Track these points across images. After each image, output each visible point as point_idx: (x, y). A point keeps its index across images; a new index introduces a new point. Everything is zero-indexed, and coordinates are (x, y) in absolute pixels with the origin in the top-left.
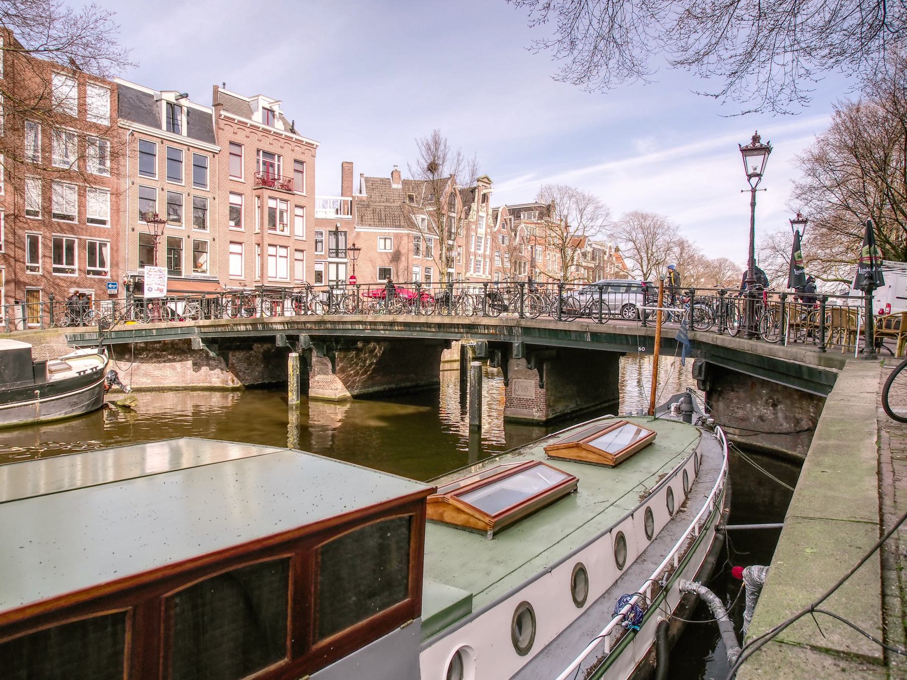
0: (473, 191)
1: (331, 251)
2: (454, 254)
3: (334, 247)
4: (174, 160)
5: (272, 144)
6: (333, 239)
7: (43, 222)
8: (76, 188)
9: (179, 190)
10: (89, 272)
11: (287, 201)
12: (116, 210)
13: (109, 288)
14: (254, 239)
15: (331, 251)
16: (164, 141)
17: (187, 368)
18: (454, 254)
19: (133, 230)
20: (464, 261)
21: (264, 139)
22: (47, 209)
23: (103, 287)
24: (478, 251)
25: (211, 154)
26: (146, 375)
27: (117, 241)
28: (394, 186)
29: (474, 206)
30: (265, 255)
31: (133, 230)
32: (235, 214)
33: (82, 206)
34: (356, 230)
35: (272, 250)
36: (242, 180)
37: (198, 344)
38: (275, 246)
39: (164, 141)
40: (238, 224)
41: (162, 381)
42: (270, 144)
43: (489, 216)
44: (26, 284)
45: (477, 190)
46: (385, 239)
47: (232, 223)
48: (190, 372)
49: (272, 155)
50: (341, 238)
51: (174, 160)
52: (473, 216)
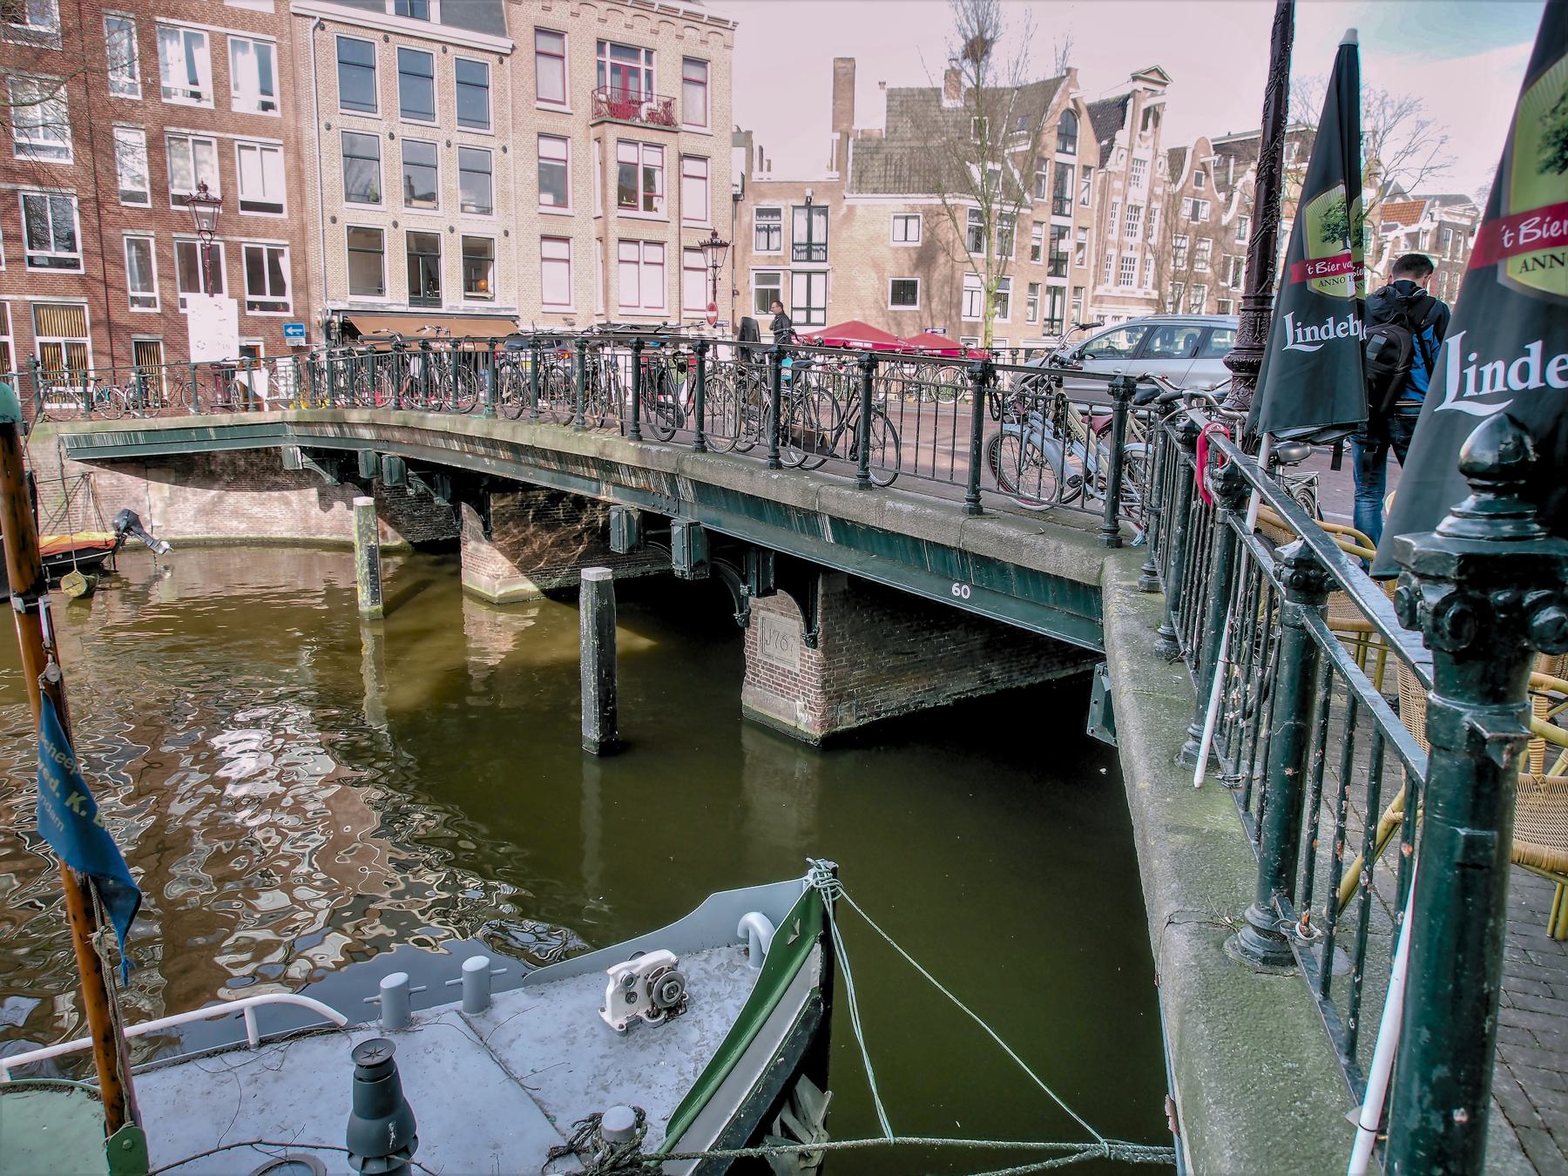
0: (1122, 104)
1: (799, 248)
2: (1066, 245)
3: (805, 240)
4: (415, 71)
5: (632, 27)
6: (801, 219)
7: (149, 214)
8: (214, 142)
9: (429, 135)
10: (252, 306)
11: (661, 146)
12: (297, 177)
13: (288, 334)
14: (594, 229)
15: (799, 248)
16: (390, 36)
17: (310, 503)
18: (1066, 245)
19: (334, 220)
20: (1093, 262)
21: (612, 16)
22: (160, 187)
23: (277, 332)
24: (1126, 239)
25: (495, 58)
26: (237, 513)
27: (304, 242)
28: (947, 103)
29: (1122, 137)
30: (613, 261)
31: (334, 220)
32: (553, 179)
33: (228, 173)
34: (847, 202)
35: (628, 251)
36: (566, 109)
37: (293, 455)
38: (636, 242)
39: (390, 36)
40: (561, 201)
41: (268, 527)
42: (627, 26)
43: (1160, 159)
44: (129, 330)
45: (1130, 101)
46: (907, 218)
47: (548, 198)
48: (316, 511)
49: (632, 51)
50: (818, 220)
51: (415, 71)
52: (1116, 163)
